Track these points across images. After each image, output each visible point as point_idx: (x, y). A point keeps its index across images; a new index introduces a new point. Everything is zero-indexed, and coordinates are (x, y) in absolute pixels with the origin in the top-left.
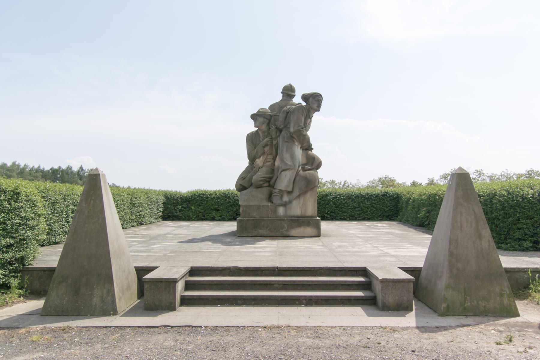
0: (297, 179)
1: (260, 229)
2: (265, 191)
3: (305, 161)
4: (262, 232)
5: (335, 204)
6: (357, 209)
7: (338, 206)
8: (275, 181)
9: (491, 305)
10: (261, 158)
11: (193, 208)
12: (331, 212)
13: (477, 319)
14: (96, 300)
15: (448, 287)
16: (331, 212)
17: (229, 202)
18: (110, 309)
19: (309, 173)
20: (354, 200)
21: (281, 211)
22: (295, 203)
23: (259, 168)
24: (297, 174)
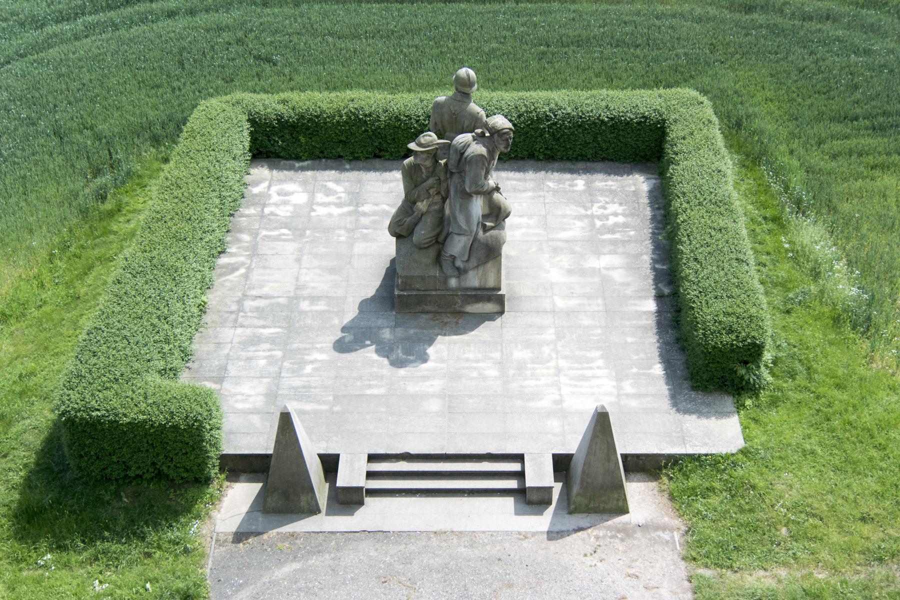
0: (476, 245)
1: (426, 305)
2: (432, 253)
3: (487, 211)
4: (428, 308)
5: (553, 135)
6: (591, 145)
7: (558, 139)
8: (446, 238)
9: (608, 506)
10: (425, 202)
11: (303, 140)
12: (547, 148)
13: (594, 517)
14: (303, 503)
15: (577, 495)
16: (547, 148)
17: (366, 131)
18: (314, 510)
19: (491, 236)
20: (586, 129)
21: (453, 282)
22: (471, 274)
23: (422, 215)
24: (475, 239)
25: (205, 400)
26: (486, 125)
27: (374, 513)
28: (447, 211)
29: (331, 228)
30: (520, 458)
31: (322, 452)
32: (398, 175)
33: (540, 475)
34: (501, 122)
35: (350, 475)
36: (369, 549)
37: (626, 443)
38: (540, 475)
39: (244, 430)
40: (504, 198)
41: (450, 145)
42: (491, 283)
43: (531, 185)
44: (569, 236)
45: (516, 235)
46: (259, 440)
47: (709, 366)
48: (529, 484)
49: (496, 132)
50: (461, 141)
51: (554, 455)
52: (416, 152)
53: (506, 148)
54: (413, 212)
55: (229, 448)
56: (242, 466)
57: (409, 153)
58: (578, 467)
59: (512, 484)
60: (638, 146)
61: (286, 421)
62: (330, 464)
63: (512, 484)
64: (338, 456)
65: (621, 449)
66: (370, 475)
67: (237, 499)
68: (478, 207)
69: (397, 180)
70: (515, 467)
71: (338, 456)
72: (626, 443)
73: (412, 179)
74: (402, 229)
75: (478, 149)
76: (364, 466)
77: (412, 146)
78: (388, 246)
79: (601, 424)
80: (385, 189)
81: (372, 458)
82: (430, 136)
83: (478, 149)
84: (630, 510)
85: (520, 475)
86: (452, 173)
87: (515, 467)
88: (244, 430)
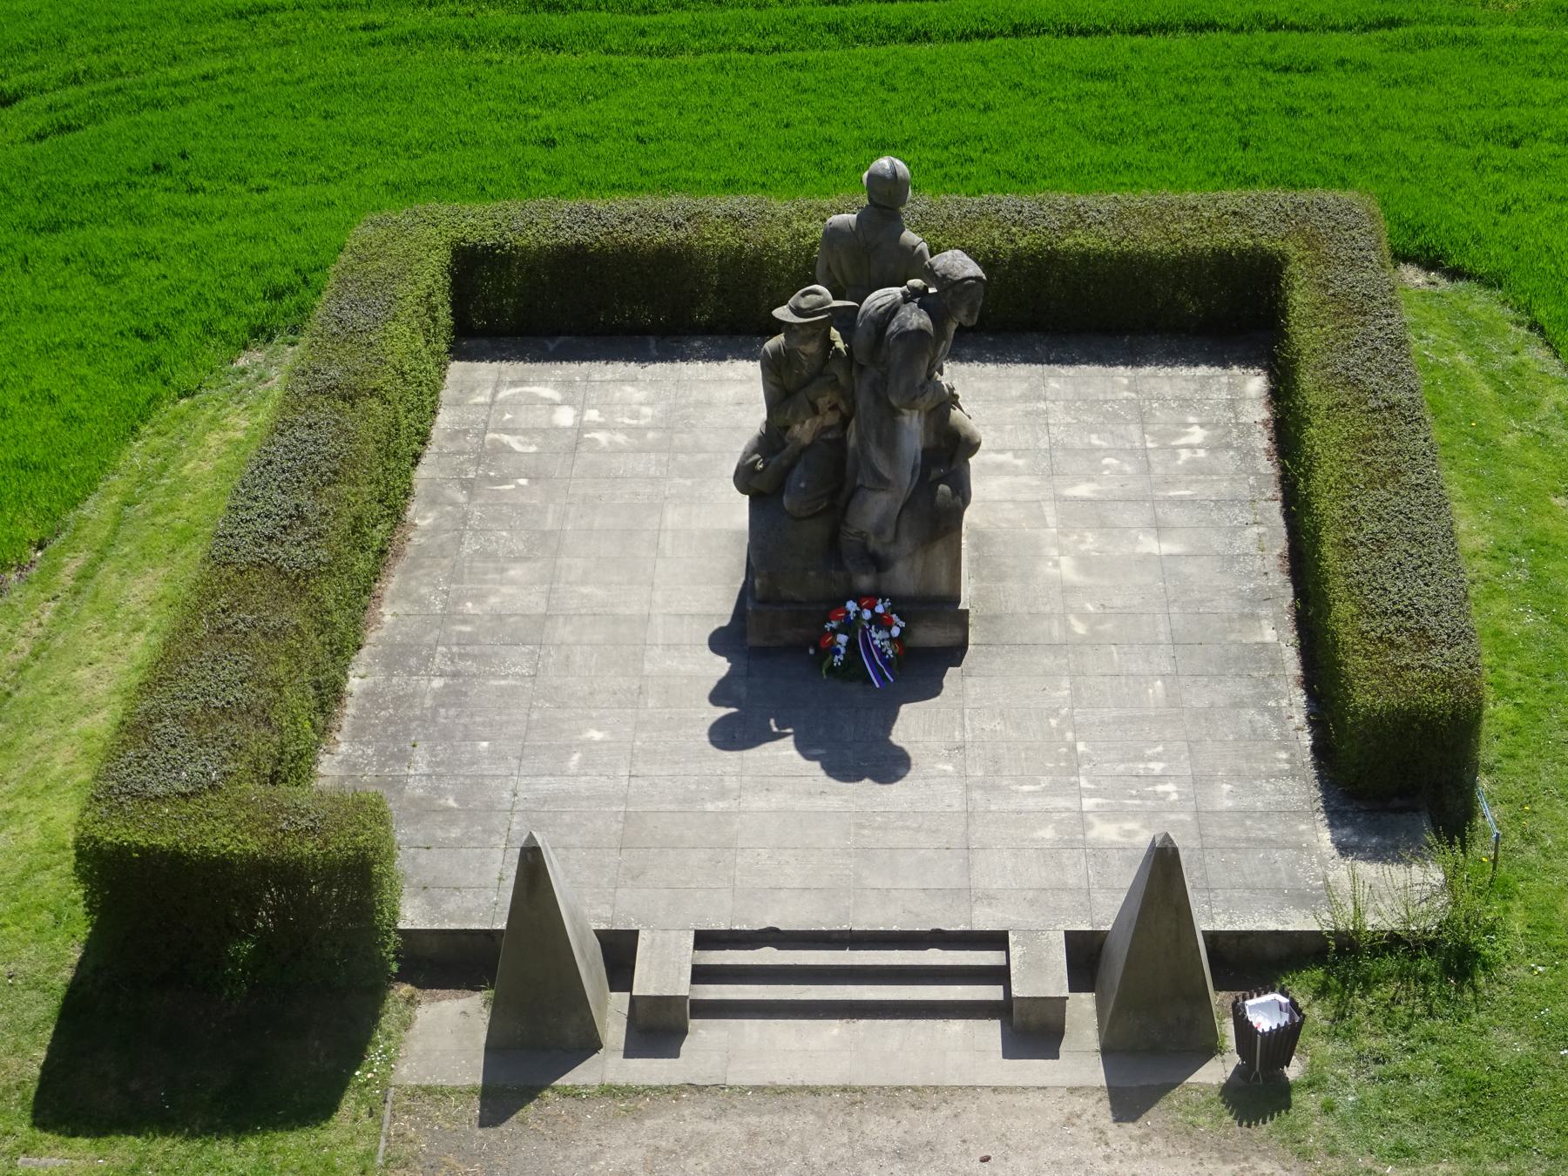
25: (370, 811)
26: (929, 274)
27: (710, 1048)
28: (852, 441)
29: (630, 483)
30: (998, 940)
31: (603, 927)
32: (751, 370)
33: (1040, 973)
34: (959, 264)
35: (663, 970)
36: (690, 1120)
37: (1214, 913)
38: (1040, 973)
39: (446, 887)
40: (972, 414)
41: (855, 310)
42: (943, 588)
43: (1018, 389)
44: (1100, 498)
45: (994, 492)
46: (484, 905)
47: (1394, 769)
48: (1016, 991)
49: (952, 287)
50: (878, 303)
51: (1071, 937)
52: (790, 324)
53: (970, 315)
54: (784, 446)
55: (412, 915)
56: (450, 961)
57: (778, 327)
58: (1118, 954)
59: (993, 993)
60: (1213, 308)
61: (532, 867)
62: (619, 951)
63: (993, 993)
64: (634, 934)
65: (1202, 925)
66: (701, 974)
67: (439, 1036)
68: (913, 430)
69: (751, 379)
70: (990, 958)
71: (634, 934)
72: (1214, 913)
73: (775, 369)
74: (762, 479)
75: (915, 318)
76: (686, 955)
77: (782, 313)
78: (738, 511)
79: (1163, 866)
80: (727, 398)
81: (705, 940)
82: (817, 293)
83: (915, 318)
84: (445, 255)
85: (1000, 975)
86: (861, 368)
87: (990, 958)
88: (446, 887)
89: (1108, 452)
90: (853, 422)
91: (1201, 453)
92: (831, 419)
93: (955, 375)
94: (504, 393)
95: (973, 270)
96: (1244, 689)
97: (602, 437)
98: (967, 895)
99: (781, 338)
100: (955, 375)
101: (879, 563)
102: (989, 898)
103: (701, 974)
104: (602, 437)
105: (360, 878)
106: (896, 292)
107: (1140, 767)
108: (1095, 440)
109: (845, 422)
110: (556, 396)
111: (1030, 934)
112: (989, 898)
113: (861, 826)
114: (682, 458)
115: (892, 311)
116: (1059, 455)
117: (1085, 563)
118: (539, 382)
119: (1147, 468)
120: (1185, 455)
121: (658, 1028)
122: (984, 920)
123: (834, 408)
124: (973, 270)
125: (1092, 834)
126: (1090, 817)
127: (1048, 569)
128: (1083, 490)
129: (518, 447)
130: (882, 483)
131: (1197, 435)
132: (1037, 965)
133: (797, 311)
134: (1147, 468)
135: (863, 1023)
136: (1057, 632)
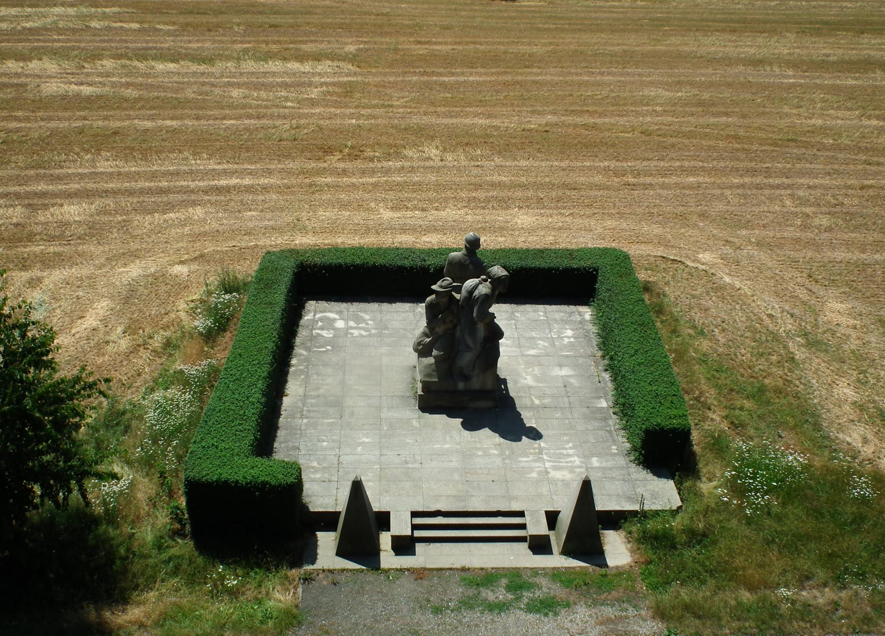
27: (426, 556)
30: (521, 514)
34: (498, 271)
35: (401, 526)
37: (601, 504)
57: (434, 292)
71: (389, 512)
72: (601, 504)
79: (586, 488)
80: (409, 319)
81: (414, 514)
88: (325, 494)
89: (540, 339)
90: (458, 328)
91: (572, 340)
92: (450, 325)
93: (494, 309)
94: (318, 316)
95: (505, 273)
96: (596, 424)
97: (356, 333)
98: (510, 498)
99: (434, 296)
100: (494, 309)
101: (466, 378)
102: (516, 498)
103: (415, 527)
104: (356, 333)
105: (291, 490)
106: (477, 280)
107: (565, 452)
108: (534, 334)
109: (455, 326)
110: (337, 317)
111: (534, 513)
112: (516, 498)
113: (467, 473)
114: (385, 339)
115: (476, 287)
116: (521, 339)
117: (537, 379)
118: (330, 311)
119: (553, 344)
120: (566, 340)
121: (403, 546)
122: (515, 507)
123: (451, 321)
124: (505, 273)
125: (550, 476)
126: (549, 470)
127: (523, 381)
128: (532, 352)
129: (325, 335)
130: (469, 348)
131: (569, 333)
132: (538, 522)
133: (441, 287)
134: (553, 344)
135: (481, 544)
136: (529, 403)
